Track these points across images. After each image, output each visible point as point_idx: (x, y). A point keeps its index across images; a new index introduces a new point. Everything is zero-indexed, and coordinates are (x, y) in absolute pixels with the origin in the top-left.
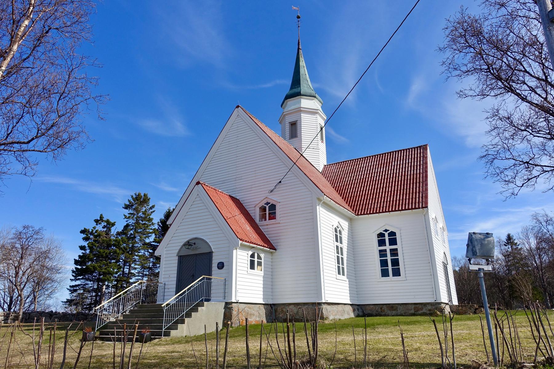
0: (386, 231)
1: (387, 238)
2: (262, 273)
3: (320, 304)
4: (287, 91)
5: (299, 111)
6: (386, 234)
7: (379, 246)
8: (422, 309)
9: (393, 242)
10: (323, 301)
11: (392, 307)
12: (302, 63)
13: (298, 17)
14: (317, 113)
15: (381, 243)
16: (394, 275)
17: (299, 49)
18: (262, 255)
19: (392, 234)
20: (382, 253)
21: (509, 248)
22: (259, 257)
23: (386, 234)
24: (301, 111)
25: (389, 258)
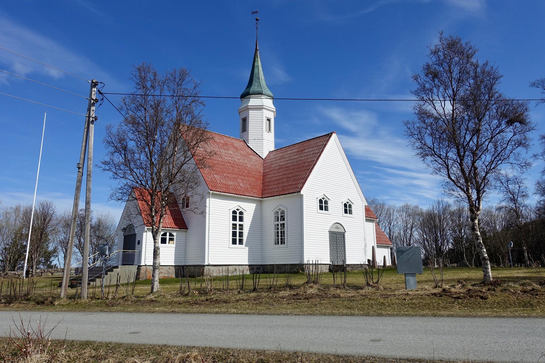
0: (238, 210)
1: (238, 215)
2: (174, 245)
3: (204, 266)
4: (242, 91)
5: (247, 109)
6: (238, 212)
7: (233, 220)
8: (294, 268)
9: (241, 219)
10: (206, 263)
11: (279, 266)
12: (259, 63)
13: (257, 20)
14: (262, 108)
15: (234, 218)
16: (281, 244)
17: (256, 50)
18: (175, 234)
20: (234, 226)
21: (512, 205)
22: (171, 235)
23: (238, 212)
24: (249, 108)
25: (238, 231)
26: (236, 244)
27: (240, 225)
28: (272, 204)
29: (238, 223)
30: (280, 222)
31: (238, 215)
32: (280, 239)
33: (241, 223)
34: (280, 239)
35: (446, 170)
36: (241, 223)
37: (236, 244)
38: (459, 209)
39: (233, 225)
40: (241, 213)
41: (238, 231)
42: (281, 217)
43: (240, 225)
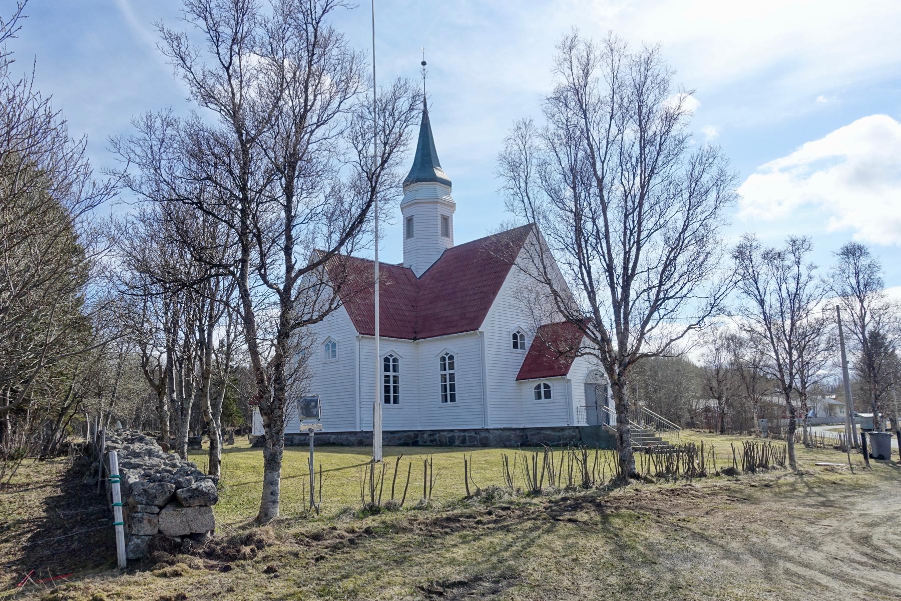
1: (391, 363)
7: (453, 374)
9: (452, 366)
15: (387, 368)
19: (451, 358)
20: (444, 377)
25: (391, 384)
26: (446, 401)
27: (394, 377)
28: (433, 349)
29: (448, 372)
30: (448, 372)
31: (391, 363)
32: (449, 393)
33: (395, 374)
34: (449, 393)
35: (379, 228)
36: (395, 374)
37: (446, 401)
38: (754, 361)
39: (386, 376)
40: (395, 360)
41: (391, 384)
42: (447, 362)
43: (394, 377)
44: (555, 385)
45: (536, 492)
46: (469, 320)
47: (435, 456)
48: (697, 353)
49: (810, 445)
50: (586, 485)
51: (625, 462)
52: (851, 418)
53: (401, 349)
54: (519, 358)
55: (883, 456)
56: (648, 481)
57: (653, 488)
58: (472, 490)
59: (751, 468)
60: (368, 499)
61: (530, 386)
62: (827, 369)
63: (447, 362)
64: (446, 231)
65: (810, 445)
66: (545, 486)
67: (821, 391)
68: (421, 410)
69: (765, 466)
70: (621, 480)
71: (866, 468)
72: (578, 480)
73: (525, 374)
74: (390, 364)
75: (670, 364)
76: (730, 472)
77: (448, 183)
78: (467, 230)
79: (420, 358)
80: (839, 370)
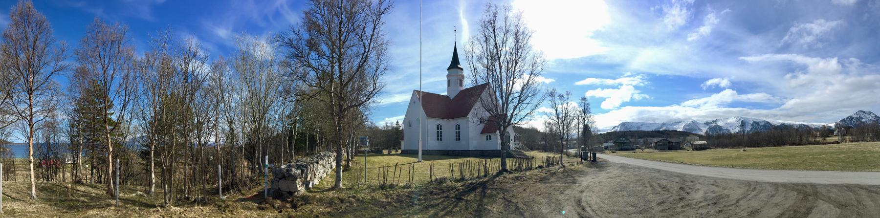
28: (453, 123)
32: (458, 138)
34: (458, 138)
42: (458, 127)
44: (493, 136)
45: (463, 179)
46: (464, 114)
47: (435, 162)
48: (541, 127)
49: (568, 155)
50: (485, 176)
51: (504, 164)
52: (579, 147)
53: (443, 122)
54: (482, 126)
55: (586, 159)
56: (510, 173)
57: (511, 176)
58: (433, 178)
59: (548, 166)
60: (382, 182)
61: (485, 136)
62: (574, 132)
63: (458, 127)
64: (461, 84)
65: (568, 155)
66: (467, 177)
67: (572, 140)
68: (449, 142)
69: (553, 164)
70: (500, 173)
71: (582, 163)
72: (482, 174)
73: (483, 132)
74: (439, 127)
75: (533, 132)
76: (541, 167)
77: (462, 69)
78: (468, 83)
79: (449, 126)
80: (33, 103)
